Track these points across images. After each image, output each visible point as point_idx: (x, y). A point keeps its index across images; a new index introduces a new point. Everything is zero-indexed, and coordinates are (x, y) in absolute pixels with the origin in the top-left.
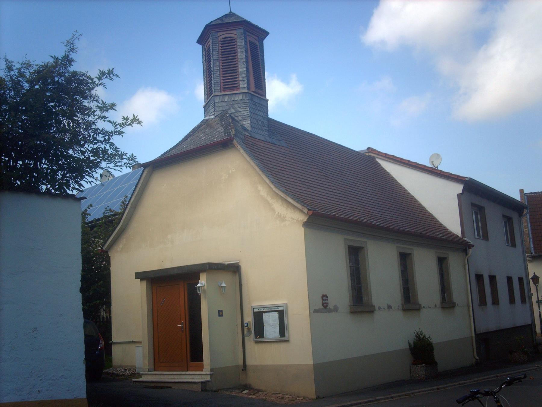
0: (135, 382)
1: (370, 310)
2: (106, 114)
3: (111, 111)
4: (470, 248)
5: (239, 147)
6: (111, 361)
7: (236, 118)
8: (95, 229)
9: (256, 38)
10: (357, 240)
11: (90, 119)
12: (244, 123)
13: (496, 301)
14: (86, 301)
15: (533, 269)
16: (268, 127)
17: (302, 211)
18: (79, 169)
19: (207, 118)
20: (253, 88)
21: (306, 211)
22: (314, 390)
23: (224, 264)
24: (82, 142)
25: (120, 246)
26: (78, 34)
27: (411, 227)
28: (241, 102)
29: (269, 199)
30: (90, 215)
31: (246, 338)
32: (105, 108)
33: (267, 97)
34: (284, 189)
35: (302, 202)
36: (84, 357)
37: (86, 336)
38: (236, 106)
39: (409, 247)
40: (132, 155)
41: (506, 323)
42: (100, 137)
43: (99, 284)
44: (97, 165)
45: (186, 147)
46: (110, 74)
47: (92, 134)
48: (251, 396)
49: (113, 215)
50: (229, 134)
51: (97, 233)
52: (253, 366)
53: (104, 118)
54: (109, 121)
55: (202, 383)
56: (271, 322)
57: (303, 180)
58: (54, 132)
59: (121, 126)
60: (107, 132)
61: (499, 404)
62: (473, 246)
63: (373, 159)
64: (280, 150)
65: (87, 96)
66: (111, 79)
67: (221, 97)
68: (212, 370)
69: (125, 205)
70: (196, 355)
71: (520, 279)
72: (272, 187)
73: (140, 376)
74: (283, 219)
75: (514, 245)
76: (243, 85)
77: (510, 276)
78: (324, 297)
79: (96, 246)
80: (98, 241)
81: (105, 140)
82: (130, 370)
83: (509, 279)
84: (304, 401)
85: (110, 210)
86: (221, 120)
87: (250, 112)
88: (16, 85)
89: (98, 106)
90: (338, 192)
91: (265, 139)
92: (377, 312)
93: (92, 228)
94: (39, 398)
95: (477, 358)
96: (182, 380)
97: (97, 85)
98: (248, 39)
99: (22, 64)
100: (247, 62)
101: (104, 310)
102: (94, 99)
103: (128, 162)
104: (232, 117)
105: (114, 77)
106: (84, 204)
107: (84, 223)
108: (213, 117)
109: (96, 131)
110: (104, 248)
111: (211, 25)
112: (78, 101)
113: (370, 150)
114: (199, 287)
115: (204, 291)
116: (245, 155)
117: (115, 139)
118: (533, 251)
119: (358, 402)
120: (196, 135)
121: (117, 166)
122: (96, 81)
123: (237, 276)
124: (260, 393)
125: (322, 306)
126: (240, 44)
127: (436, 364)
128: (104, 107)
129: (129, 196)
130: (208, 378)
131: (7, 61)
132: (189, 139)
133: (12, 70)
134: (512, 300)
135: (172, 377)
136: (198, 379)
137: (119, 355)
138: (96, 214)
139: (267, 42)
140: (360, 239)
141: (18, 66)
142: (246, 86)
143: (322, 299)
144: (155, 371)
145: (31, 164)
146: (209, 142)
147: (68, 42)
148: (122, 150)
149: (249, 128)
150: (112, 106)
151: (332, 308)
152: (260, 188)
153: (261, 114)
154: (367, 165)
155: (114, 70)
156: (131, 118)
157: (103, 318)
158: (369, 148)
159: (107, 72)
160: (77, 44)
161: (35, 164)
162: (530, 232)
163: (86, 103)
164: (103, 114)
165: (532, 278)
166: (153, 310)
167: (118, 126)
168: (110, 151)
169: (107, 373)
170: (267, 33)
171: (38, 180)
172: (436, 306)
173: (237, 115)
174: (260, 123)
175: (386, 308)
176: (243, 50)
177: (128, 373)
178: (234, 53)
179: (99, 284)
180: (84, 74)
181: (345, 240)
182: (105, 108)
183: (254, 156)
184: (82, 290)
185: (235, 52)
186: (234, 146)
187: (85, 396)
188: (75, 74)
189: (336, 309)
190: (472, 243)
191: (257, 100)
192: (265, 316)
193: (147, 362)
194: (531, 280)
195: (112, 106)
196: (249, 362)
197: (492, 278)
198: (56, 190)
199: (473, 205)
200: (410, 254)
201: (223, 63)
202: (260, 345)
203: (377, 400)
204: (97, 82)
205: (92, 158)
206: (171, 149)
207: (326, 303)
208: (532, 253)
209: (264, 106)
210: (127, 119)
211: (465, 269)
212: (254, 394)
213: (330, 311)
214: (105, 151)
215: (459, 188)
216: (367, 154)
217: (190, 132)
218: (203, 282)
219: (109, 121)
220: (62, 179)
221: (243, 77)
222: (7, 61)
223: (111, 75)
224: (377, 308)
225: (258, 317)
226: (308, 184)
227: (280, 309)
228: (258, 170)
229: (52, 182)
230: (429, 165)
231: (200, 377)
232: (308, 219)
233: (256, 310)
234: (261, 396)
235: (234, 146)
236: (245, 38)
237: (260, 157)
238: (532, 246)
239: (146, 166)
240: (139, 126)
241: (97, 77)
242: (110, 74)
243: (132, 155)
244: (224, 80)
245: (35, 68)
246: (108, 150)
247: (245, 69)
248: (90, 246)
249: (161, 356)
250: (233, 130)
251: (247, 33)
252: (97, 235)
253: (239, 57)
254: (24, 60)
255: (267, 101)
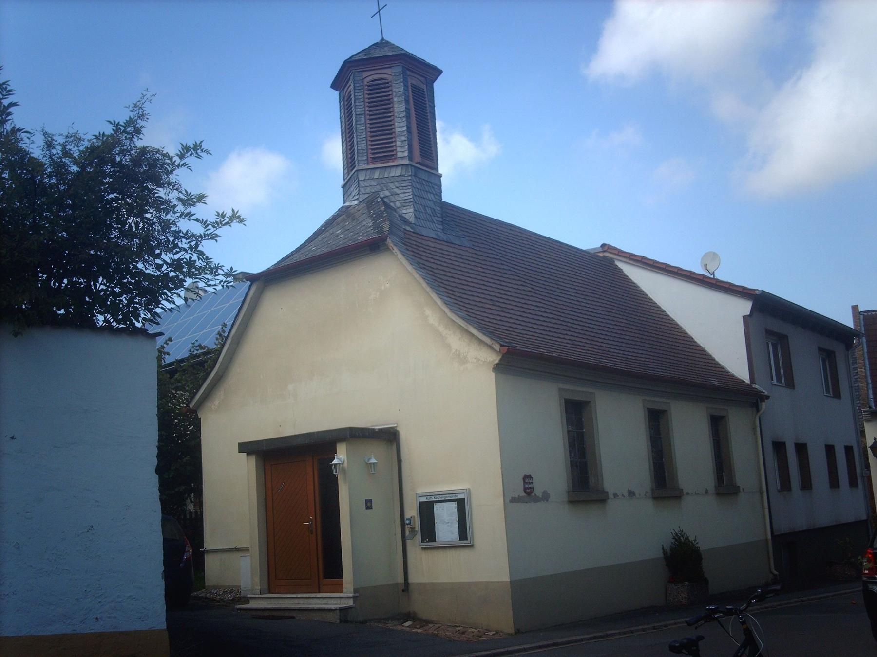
0: (240, 609)
1: (600, 498)
2: (192, 210)
3: (199, 205)
4: (762, 400)
5: (396, 250)
6: (203, 578)
7: (392, 204)
8: (177, 376)
9: (423, 79)
10: (578, 391)
11: (168, 217)
12: (404, 211)
13: (806, 484)
14: (164, 486)
15: (874, 432)
16: (442, 217)
17: (491, 348)
18: (153, 290)
19: (347, 204)
20: (417, 157)
21: (497, 347)
22: (511, 621)
23: (374, 429)
24: (157, 251)
25: (216, 401)
26: (149, 94)
27: (667, 368)
28: (400, 179)
29: (441, 329)
30: (168, 354)
31: (408, 542)
32: (190, 201)
33: (440, 171)
34: (464, 314)
35: (491, 334)
36: (162, 569)
37: (165, 541)
38: (391, 185)
39: (665, 400)
40: (232, 268)
41: (824, 518)
42: (184, 244)
43: (184, 460)
44: (179, 284)
45: (314, 250)
46: (196, 149)
47: (171, 239)
48: (415, 630)
49: (204, 354)
50: (380, 229)
51: (179, 381)
52: (421, 584)
53: (189, 215)
54: (197, 220)
55: (341, 610)
56: (446, 519)
57: (496, 299)
58: (115, 237)
59: (214, 227)
60: (193, 235)
61: (745, 626)
62: (767, 397)
63: (611, 262)
64: (461, 252)
65: (163, 184)
66: (199, 157)
67: (369, 172)
68: (355, 591)
69: (222, 338)
70: (332, 568)
71: (849, 450)
72: (446, 310)
73: (247, 600)
74: (463, 360)
75: (837, 395)
76: (402, 152)
77: (830, 443)
78: (527, 478)
79: (178, 401)
80: (182, 395)
81: (191, 248)
82: (231, 592)
83: (830, 449)
84: (497, 637)
85: (200, 346)
86: (368, 208)
87: (414, 195)
88: (59, 168)
89: (179, 199)
90: (551, 316)
91: (437, 234)
92: (611, 503)
93: (172, 373)
94: (98, 628)
95: (776, 573)
96: (311, 606)
97: (178, 166)
98: (411, 81)
99: (67, 137)
100: (408, 117)
101: (191, 501)
102: (173, 187)
103: (224, 279)
104: (384, 203)
105: (203, 154)
106: (160, 340)
107: (160, 366)
108: (356, 202)
109: (177, 234)
110: (191, 407)
111: (351, 62)
112: (150, 191)
113: (606, 248)
114: (335, 465)
115: (344, 471)
116: (405, 262)
117: (206, 247)
118: (872, 404)
119: (578, 637)
120: (331, 231)
121: (209, 286)
122: (177, 159)
123: (395, 446)
124: (430, 625)
125: (524, 492)
126: (397, 90)
127: (706, 581)
128: (188, 200)
129: (229, 324)
130: (351, 603)
131: (45, 134)
132: (320, 238)
133: (54, 148)
134: (834, 483)
135: (296, 601)
136: (334, 605)
137: (215, 570)
138: (178, 352)
139: (439, 86)
140: (584, 390)
141: (61, 140)
142: (406, 154)
143: (525, 482)
144: (270, 592)
145: (81, 283)
146: (350, 243)
147: (135, 105)
148: (215, 261)
149: (412, 220)
150: (201, 198)
151: (539, 495)
152: (428, 312)
153: (431, 197)
154: (600, 275)
155: (203, 144)
156: (229, 213)
157: (191, 513)
158: (603, 245)
159: (192, 146)
160: (148, 108)
161: (88, 283)
162: (868, 373)
163: (161, 192)
164: (188, 210)
165: (871, 447)
166: (266, 499)
167: (210, 227)
168: (199, 263)
169: (197, 598)
170: (440, 72)
171: (91, 306)
172: (707, 492)
173: (393, 199)
174: (429, 211)
175: (626, 494)
176: (402, 98)
177: (229, 597)
178: (387, 102)
179: (184, 460)
180: (158, 151)
181: (560, 390)
182: (190, 201)
183: (419, 263)
184: (158, 470)
185: (389, 102)
186: (387, 249)
187: (164, 626)
188: (144, 151)
189: (546, 497)
190: (766, 393)
191: (423, 176)
192: (437, 508)
193: (257, 579)
194: (869, 450)
195: (201, 198)
196: (414, 578)
197: (801, 448)
198: (119, 322)
199: (769, 333)
200: (665, 411)
201: (371, 120)
202: (429, 552)
203: (607, 635)
204: (177, 163)
205: (172, 274)
206: (292, 253)
207: (530, 488)
208: (870, 407)
209: (435, 185)
210: (223, 216)
211: (755, 434)
212: (421, 627)
213: (537, 500)
214: (190, 263)
215: (745, 307)
216: (601, 255)
217: (322, 226)
218: (341, 456)
219: (197, 220)
220: (128, 305)
221: (403, 141)
222: (45, 134)
223: (199, 151)
224: (611, 496)
225: (427, 509)
226: (504, 305)
227: (460, 496)
228: (424, 285)
229: (114, 309)
230: (699, 270)
231: (338, 601)
232: (500, 360)
233: (423, 499)
234: (431, 629)
235: (387, 249)
236: (405, 82)
237: (429, 265)
238: (871, 396)
239: (252, 278)
240: (241, 225)
241: (177, 155)
242: (196, 149)
243: (232, 268)
244: (372, 145)
245: (86, 144)
246: (195, 261)
247: (405, 129)
248: (168, 402)
249: (280, 571)
250: (388, 223)
251: (408, 73)
252: (179, 385)
253: (396, 110)
254: (71, 131)
255: (440, 176)
